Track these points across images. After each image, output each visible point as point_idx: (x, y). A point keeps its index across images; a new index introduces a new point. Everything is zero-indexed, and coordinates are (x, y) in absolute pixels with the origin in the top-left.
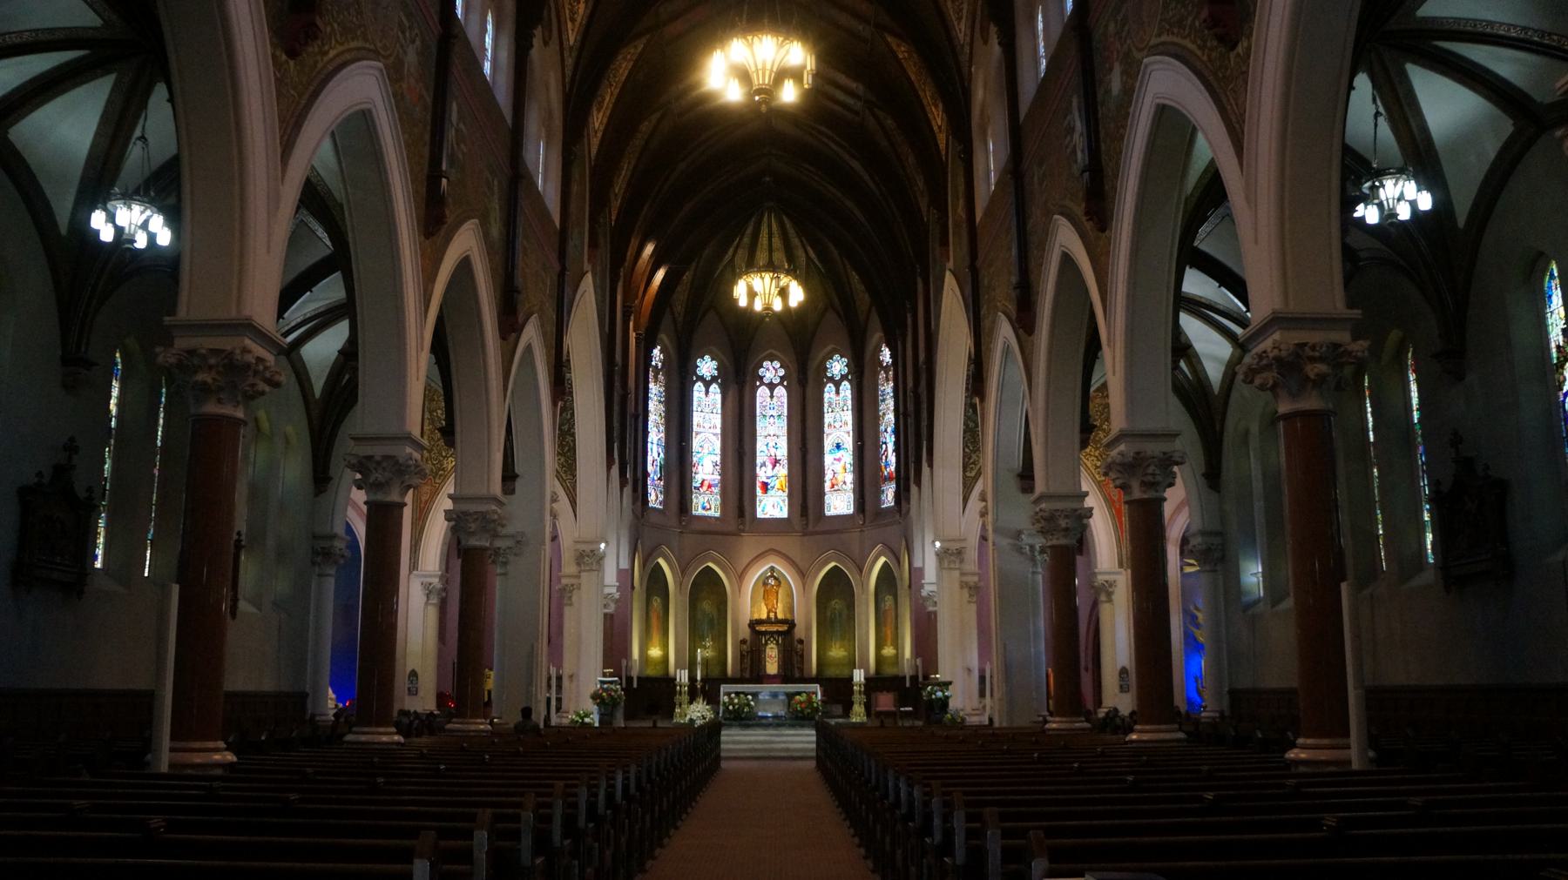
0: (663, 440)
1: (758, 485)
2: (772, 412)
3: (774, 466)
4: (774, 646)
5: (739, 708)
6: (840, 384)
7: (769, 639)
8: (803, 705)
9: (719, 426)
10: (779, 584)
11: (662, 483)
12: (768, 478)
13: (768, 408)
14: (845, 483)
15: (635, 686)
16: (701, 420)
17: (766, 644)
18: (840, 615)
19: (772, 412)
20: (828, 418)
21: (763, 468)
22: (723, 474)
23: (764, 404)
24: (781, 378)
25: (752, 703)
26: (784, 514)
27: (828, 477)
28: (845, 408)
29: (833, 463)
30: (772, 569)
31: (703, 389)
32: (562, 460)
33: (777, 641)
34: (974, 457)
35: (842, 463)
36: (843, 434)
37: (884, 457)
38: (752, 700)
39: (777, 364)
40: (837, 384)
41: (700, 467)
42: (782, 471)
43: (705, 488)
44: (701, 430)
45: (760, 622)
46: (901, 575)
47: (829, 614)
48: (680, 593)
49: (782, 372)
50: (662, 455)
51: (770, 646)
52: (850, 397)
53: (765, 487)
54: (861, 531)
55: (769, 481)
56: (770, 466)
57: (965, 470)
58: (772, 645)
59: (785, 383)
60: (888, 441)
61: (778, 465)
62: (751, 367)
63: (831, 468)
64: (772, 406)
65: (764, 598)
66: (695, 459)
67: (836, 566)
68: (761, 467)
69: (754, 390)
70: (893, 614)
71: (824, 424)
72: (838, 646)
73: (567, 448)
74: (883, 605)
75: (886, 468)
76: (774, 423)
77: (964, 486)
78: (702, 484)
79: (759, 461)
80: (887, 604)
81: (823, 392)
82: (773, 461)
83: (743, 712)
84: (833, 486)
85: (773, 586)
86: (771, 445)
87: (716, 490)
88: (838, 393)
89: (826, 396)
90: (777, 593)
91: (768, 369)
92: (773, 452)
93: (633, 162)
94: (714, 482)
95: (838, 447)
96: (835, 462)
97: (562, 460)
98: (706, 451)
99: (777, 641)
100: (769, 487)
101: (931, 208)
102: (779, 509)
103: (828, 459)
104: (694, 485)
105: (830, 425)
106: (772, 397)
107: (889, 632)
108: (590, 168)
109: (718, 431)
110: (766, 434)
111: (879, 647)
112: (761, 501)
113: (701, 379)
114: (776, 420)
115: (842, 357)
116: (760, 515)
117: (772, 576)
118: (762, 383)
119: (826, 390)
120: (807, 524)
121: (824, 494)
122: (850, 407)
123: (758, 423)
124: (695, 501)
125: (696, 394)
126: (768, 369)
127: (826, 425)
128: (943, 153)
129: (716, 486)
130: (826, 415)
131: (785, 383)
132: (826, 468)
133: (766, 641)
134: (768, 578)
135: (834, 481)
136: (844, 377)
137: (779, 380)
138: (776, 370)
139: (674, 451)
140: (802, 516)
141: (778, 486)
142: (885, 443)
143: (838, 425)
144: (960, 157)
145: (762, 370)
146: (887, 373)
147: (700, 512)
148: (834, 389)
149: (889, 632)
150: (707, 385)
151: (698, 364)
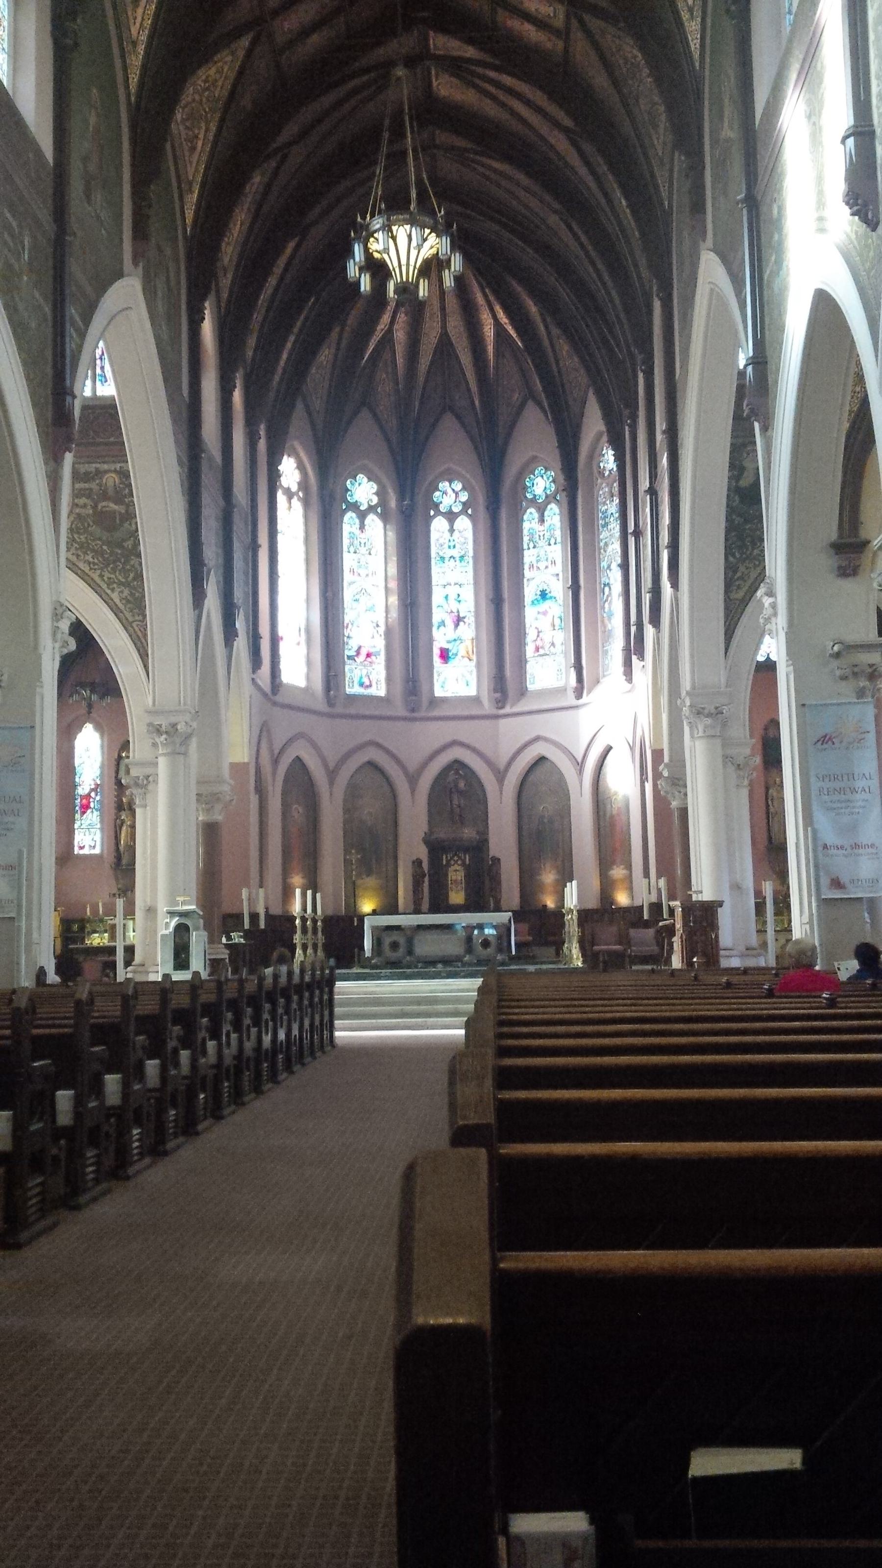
1: (436, 652)
3: (457, 625)
6: (544, 510)
7: (451, 858)
12: (449, 642)
13: (446, 546)
14: (553, 644)
15: (262, 925)
16: (355, 566)
17: (448, 865)
20: (529, 556)
27: (531, 635)
28: (552, 541)
31: (357, 521)
32: (126, 592)
34: (742, 569)
39: (458, 486)
40: (541, 510)
42: (467, 631)
43: (362, 657)
51: (452, 868)
52: (558, 525)
53: (445, 655)
56: (452, 626)
57: (727, 592)
59: (470, 511)
61: (461, 623)
68: (439, 627)
69: (428, 520)
73: (132, 575)
77: (727, 616)
78: (358, 652)
79: (436, 618)
82: (455, 619)
84: (537, 649)
88: (542, 520)
89: (526, 526)
91: (445, 493)
92: (454, 606)
93: (213, 127)
95: (544, 595)
96: (540, 616)
97: (126, 592)
100: (450, 654)
101: (677, 154)
103: (530, 613)
104: (347, 653)
105: (531, 566)
106: (452, 530)
108: (129, 111)
113: (355, 507)
115: (546, 469)
118: (438, 513)
119: (525, 517)
121: (526, 661)
122: (559, 540)
124: (348, 675)
126: (445, 493)
127: (526, 567)
128: (696, 56)
130: (526, 553)
131: (470, 511)
132: (527, 626)
133: (448, 861)
135: (539, 643)
136: (549, 499)
137: (460, 508)
138: (457, 494)
143: (542, 565)
144: (728, 11)
145: (437, 494)
147: (356, 690)
148: (536, 515)
151: (349, 487)
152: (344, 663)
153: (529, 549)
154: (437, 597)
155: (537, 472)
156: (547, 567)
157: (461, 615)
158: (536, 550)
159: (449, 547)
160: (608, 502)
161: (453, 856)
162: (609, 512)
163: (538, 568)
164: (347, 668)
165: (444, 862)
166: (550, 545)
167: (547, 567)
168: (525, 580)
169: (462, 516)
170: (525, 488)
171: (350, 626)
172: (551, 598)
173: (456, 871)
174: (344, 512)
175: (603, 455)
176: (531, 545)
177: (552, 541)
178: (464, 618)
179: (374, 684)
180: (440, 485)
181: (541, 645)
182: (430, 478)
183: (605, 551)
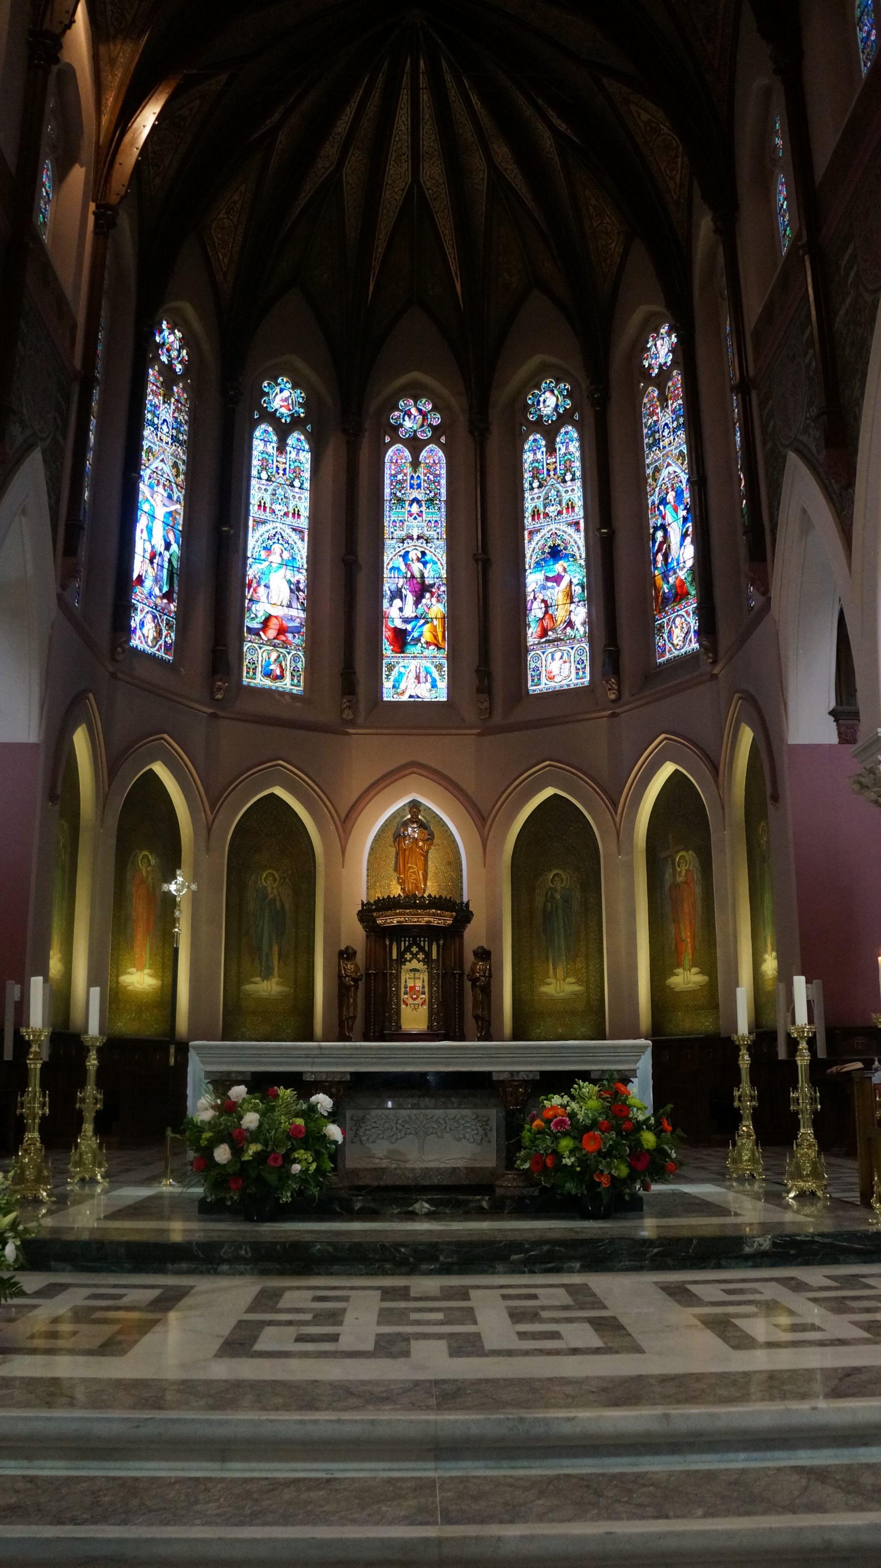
0: (180, 519)
1: (386, 633)
2: (415, 494)
4: (420, 966)
5: (260, 1157)
6: (557, 432)
7: (408, 949)
8: (590, 1146)
9: (305, 513)
10: (430, 839)
11: (173, 607)
12: (406, 621)
14: (570, 624)
16: (268, 498)
17: (401, 960)
18: (567, 901)
19: (415, 494)
20: (531, 501)
21: (397, 603)
22: (311, 607)
23: (400, 477)
24: (434, 429)
25: (334, 1131)
26: (441, 694)
27: (536, 611)
28: (568, 477)
29: (544, 587)
30: (415, 806)
33: (428, 955)
35: (565, 583)
36: (564, 527)
37: (660, 557)
38: (334, 1116)
41: (262, 590)
43: (272, 633)
44: (267, 515)
45: (389, 904)
46: (723, 804)
47: (539, 901)
48: (208, 849)
49: (436, 419)
50: (175, 548)
51: (408, 966)
54: (614, 715)
55: (409, 627)
56: (410, 598)
58: (415, 964)
59: (443, 440)
60: (669, 518)
61: (428, 595)
62: (373, 407)
63: (540, 597)
64: (415, 482)
65: (396, 869)
66: (251, 573)
67: (555, 796)
68: (392, 600)
70: (698, 890)
71: (523, 511)
72: (560, 972)
74: (668, 872)
75: (665, 578)
76: (420, 514)
79: (388, 586)
80: (683, 869)
81: (522, 451)
83: (285, 1175)
84: (544, 633)
85: (416, 840)
86: (413, 555)
87: (297, 640)
88: (551, 450)
89: (528, 457)
90: (426, 857)
91: (408, 412)
94: (291, 624)
95: (555, 553)
96: (549, 584)
98: (275, 558)
99: (428, 955)
100: (409, 639)
102: (429, 685)
103: (533, 579)
104: (248, 623)
105: (535, 514)
107: (686, 934)
109: (303, 522)
110: (403, 534)
111: (659, 973)
112: (391, 668)
113: (272, 418)
114: (423, 508)
115: (558, 381)
116: (388, 695)
117: (413, 820)
118: (396, 439)
119: (526, 447)
120: (491, 711)
121: (527, 651)
123: (386, 513)
125: (258, 446)
127: (528, 514)
129: (295, 631)
131: (443, 440)
132: (530, 597)
133: (401, 954)
134: (405, 824)
136: (563, 419)
139: (203, 542)
140: (479, 690)
141: (427, 636)
142: (663, 527)
143: (552, 510)
146: (662, 387)
147: (261, 681)
149: (686, 934)
150: (283, 432)
152: (241, 640)
153: (532, 489)
154: (391, 557)
155: (544, 385)
156: (560, 513)
157: (428, 581)
158: (544, 490)
159: (412, 487)
160: (659, 410)
161: (411, 946)
162: (662, 423)
163: (546, 515)
164: (246, 646)
165: (394, 957)
166: (564, 481)
167: (560, 513)
168: (526, 533)
169: (431, 446)
170: (526, 407)
171: (254, 585)
172: (567, 556)
173: (415, 970)
174: (257, 423)
175: (649, 349)
176: (536, 484)
177: (568, 477)
178: (432, 586)
179: (288, 675)
180: (401, 403)
181: (550, 625)
182: (389, 390)
183: (655, 480)
